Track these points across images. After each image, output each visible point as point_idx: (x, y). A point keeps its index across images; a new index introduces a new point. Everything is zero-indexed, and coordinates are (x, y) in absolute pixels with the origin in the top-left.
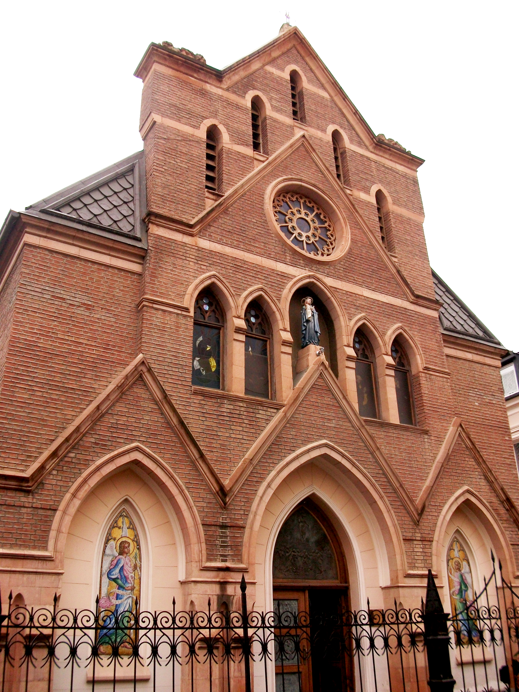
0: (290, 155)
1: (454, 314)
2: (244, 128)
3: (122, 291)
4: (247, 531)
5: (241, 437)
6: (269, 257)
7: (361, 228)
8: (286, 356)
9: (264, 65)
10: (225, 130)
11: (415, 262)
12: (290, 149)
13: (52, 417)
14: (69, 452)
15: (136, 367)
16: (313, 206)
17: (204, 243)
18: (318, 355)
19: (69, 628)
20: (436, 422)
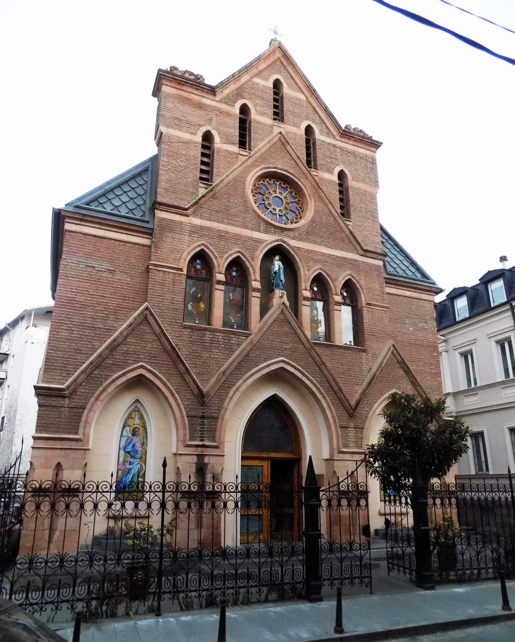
0: (269, 148)
1: (398, 262)
2: (233, 131)
3: (137, 259)
4: (220, 420)
5: (218, 357)
6: (246, 227)
7: (323, 201)
8: (256, 298)
9: (252, 78)
10: (217, 134)
11: (366, 224)
12: (269, 144)
13: (84, 347)
14: (94, 370)
15: (142, 312)
16: (287, 187)
17: (197, 221)
18: (281, 297)
19: (93, 492)
20: (372, 343)
